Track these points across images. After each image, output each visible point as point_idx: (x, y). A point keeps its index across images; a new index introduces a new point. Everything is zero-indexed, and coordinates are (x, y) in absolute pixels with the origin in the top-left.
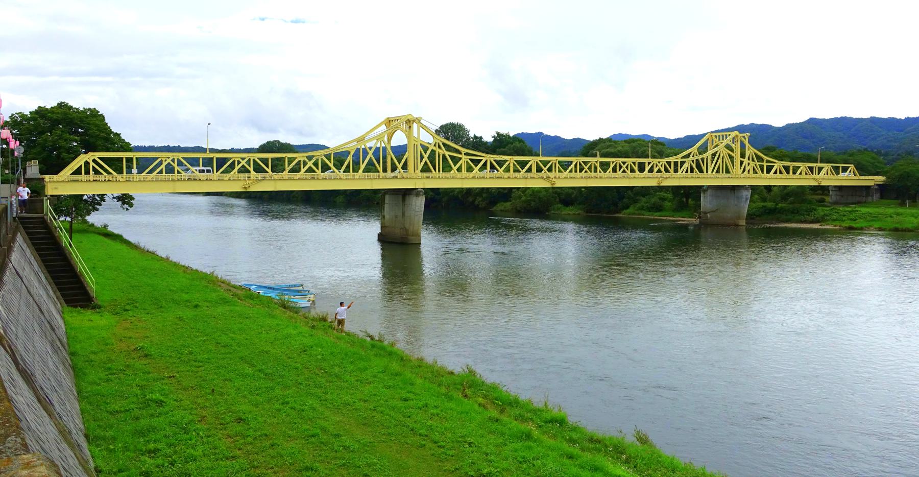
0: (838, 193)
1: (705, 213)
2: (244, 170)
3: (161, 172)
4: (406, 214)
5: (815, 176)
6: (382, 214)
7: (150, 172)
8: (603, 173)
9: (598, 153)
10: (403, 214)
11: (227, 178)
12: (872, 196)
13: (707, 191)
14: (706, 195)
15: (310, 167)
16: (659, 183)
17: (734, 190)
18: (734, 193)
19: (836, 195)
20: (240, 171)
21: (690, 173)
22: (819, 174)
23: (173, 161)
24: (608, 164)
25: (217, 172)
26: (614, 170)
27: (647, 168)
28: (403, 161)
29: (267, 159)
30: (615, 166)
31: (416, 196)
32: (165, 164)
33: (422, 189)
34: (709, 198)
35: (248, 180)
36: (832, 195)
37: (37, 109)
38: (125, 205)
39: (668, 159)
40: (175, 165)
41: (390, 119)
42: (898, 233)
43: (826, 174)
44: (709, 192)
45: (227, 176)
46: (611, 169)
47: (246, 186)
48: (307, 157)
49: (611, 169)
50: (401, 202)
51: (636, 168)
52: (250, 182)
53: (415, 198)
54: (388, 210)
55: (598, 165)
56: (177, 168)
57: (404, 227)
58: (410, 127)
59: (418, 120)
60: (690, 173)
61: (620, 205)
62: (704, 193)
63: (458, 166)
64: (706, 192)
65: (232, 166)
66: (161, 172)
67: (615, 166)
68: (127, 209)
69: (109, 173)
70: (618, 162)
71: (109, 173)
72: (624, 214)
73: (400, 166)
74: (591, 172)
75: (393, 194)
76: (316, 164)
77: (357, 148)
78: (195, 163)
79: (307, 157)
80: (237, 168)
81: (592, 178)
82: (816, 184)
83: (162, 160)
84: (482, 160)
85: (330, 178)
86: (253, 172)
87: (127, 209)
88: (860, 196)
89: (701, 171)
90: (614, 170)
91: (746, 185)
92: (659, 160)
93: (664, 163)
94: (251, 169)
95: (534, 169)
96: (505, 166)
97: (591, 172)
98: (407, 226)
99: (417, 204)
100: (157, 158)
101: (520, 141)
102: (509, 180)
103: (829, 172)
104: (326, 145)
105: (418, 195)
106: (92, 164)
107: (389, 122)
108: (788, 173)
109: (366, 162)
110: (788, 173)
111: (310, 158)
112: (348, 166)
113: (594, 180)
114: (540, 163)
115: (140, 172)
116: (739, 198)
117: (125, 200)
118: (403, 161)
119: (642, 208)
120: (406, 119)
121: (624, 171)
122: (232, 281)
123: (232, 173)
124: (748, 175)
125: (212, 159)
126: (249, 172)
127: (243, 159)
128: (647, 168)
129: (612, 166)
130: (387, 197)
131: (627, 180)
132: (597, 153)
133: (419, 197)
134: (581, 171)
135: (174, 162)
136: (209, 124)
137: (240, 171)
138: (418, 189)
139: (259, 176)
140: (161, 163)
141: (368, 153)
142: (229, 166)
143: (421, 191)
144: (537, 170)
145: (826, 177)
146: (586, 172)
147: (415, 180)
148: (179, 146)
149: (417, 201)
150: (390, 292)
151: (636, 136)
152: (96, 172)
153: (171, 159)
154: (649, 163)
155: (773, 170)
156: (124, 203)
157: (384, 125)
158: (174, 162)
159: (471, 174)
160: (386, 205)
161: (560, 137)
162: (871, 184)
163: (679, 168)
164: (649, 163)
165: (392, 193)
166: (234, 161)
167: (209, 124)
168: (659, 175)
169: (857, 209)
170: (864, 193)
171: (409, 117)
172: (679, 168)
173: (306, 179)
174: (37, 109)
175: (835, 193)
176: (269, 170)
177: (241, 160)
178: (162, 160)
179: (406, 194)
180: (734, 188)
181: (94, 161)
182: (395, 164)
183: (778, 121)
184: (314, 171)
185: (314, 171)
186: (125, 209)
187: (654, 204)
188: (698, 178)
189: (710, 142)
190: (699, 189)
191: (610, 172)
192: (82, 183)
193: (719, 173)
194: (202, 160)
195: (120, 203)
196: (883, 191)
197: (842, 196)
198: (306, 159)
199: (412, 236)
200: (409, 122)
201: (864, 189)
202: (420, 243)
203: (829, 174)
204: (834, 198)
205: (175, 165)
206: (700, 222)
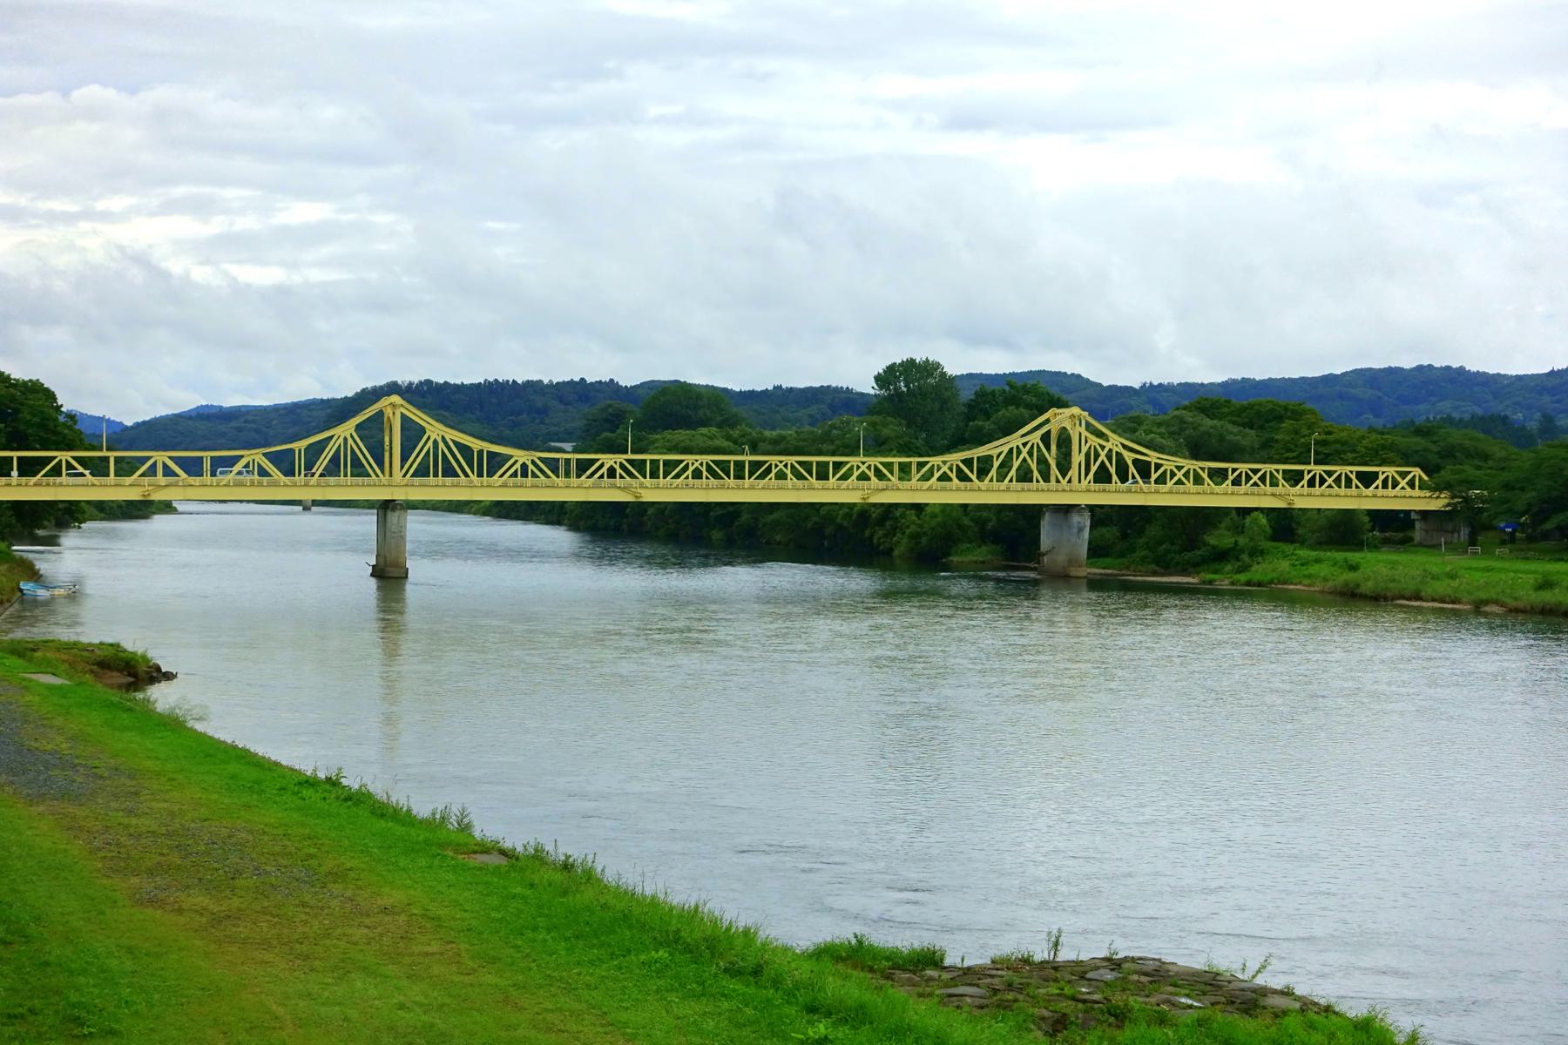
2: (863, 477)
3: (602, 476)
7: (677, 476)
11: (844, 486)
15: (1180, 479)
20: (859, 478)
21: (434, 476)
23: (701, 464)
24: (1375, 476)
25: (749, 479)
29: (891, 464)
32: (691, 469)
37: (881, 371)
40: (704, 469)
45: (762, 483)
46: (1305, 482)
48: (942, 462)
49: (1305, 482)
52: (869, 491)
55: (1353, 477)
60: (434, 476)
63: (1067, 478)
65: (769, 470)
66: (602, 476)
69: (548, 477)
70: (1344, 472)
71: (548, 477)
76: (1186, 475)
78: (125, 466)
79: (942, 462)
80: (774, 471)
81: (733, 488)
83: (688, 464)
85: (1129, 491)
86: (955, 480)
89: (1047, 479)
90: (1385, 485)
91: (1080, 505)
94: (953, 476)
97: (1340, 487)
100: (767, 462)
102: (1374, 499)
106: (531, 467)
109: (1098, 463)
111: (944, 463)
113: (735, 491)
115: (579, 476)
123: (1224, 485)
124: (1403, 493)
125: (829, 462)
126: (869, 479)
127: (697, 461)
129: (1307, 477)
131: (1256, 498)
134: (1394, 487)
135: (870, 470)
137: (859, 478)
139: (800, 483)
140: (602, 466)
141: (1028, 453)
142: (718, 467)
144: (163, 473)
146: (1330, 486)
152: (534, 475)
153: (699, 462)
154: (1309, 472)
158: (870, 470)
159: (1060, 487)
163: (519, 470)
164: (1309, 472)
166: (771, 464)
173: (442, 486)
174: (881, 371)
176: (974, 477)
177: (778, 463)
178: (688, 464)
181: (533, 462)
184: (1183, 484)
185: (1183, 484)
191: (1303, 486)
193: (1387, 488)
194: (650, 463)
198: (941, 464)
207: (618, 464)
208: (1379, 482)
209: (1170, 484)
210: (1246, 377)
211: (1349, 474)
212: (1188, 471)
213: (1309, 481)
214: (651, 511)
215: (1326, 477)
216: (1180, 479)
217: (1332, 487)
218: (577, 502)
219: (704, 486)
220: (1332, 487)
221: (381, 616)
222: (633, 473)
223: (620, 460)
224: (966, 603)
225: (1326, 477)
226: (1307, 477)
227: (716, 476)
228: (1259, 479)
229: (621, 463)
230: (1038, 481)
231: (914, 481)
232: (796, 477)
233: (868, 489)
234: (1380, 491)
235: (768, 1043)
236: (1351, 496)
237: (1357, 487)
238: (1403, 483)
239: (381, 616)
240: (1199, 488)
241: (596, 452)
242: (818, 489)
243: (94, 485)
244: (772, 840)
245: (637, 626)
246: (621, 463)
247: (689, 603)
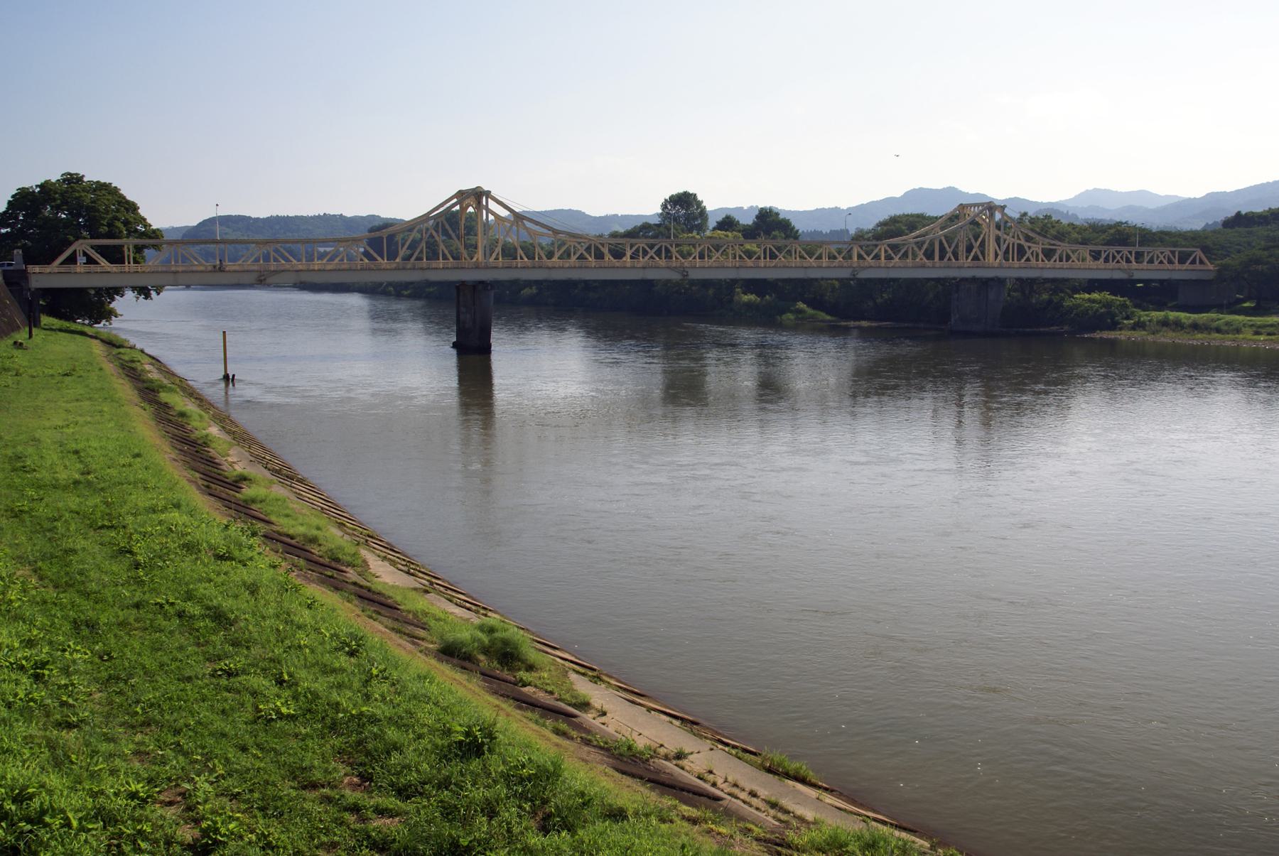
8: (1046, 262)
11: (409, 266)
26: (1106, 260)
27: (1147, 258)
28: (980, 240)
30: (1108, 255)
51: (1133, 259)
59: (488, 194)
67: (1108, 255)
74: (660, 258)
90: (1106, 260)
92: (1119, 248)
93: (641, 245)
112: (403, 246)
118: (980, 240)
121: (1118, 262)
122: (953, 446)
128: (1147, 258)
129: (1103, 256)
134: (1067, 261)
148: (684, 203)
150: (761, 395)
151: (1238, 192)
159: (774, 262)
161: (1109, 191)
163: (1189, 261)
168: (1161, 266)
172: (400, 248)
182: (944, 248)
208: (1057, 256)
209: (574, 258)
210: (32, 180)
211: (600, 247)
212: (660, 249)
213: (1105, 258)
215: (648, 249)
221: (464, 418)
222: (372, 255)
223: (643, 245)
224: (1169, 388)
225: (648, 249)
226: (1103, 256)
228: (655, 253)
230: (521, 258)
231: (1145, 263)
232: (613, 256)
234: (1191, 267)
235: (805, 855)
236: (605, 267)
238: (652, 253)
239: (464, 418)
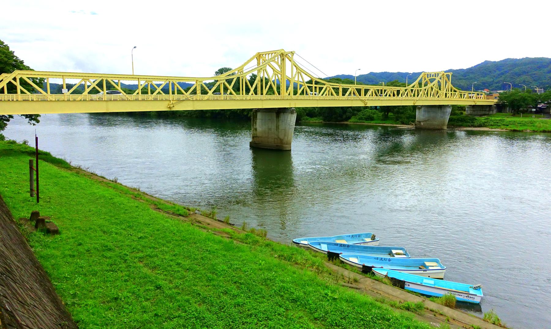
0: (471, 109)
1: (420, 122)
4: (280, 128)
5: (363, 97)
6: (254, 127)
9: (383, 83)
10: (277, 127)
12: (493, 111)
13: (421, 108)
14: (420, 111)
16: (414, 104)
17: (441, 108)
18: (441, 110)
19: (471, 110)
22: (365, 95)
31: (292, 114)
33: (294, 108)
34: (422, 113)
35: (172, 100)
36: (467, 111)
38: (32, 121)
39: (398, 88)
40: (17, 84)
41: (260, 54)
42: (545, 134)
43: (371, 95)
44: (423, 108)
47: (171, 106)
50: (275, 118)
52: (174, 102)
53: (290, 115)
54: (260, 125)
56: (19, 87)
57: (279, 138)
58: (283, 59)
61: (344, 117)
62: (419, 110)
64: (420, 109)
68: (34, 124)
72: (351, 122)
73: (252, 90)
75: (265, 112)
77: (253, 75)
82: (474, 104)
84: (323, 87)
87: (34, 124)
88: (485, 111)
95: (199, 91)
96: (207, 88)
98: (281, 137)
99: (292, 120)
101: (472, 73)
103: (374, 94)
104: (416, 71)
105: (292, 112)
107: (259, 56)
108: (337, 93)
110: (337, 93)
114: (205, 86)
116: (444, 113)
117: (33, 118)
119: (361, 119)
120: (281, 53)
130: (259, 115)
132: (382, 83)
133: (293, 114)
134: (152, 93)
136: (135, 47)
138: (291, 108)
139: (29, 95)
143: (294, 110)
144: (8, 92)
145: (371, 98)
147: (290, 101)
149: (292, 118)
155: (348, 93)
156: (30, 120)
157: (256, 58)
159: (206, 97)
160: (258, 120)
162: (492, 104)
165: (265, 111)
167: (135, 47)
169: (504, 119)
170: (488, 109)
171: (283, 52)
175: (469, 109)
179: (281, 112)
180: (440, 107)
183: (466, 66)
186: (32, 125)
187: (369, 116)
188: (378, 100)
189: (423, 79)
190: (415, 107)
191: (138, 94)
192: (33, 103)
195: (28, 119)
196: (500, 108)
197: (474, 111)
199: (287, 144)
200: (283, 56)
201: (488, 107)
202: (291, 150)
203: (373, 95)
204: (469, 112)
205: (17, 84)
206: (416, 128)
207: (18, 80)
208: (139, 90)
214: (362, 108)
216: (159, 87)
217: (161, 94)
218: (126, 112)
219: (225, 99)
220: (161, 94)
227: (32, 90)
229: (21, 79)
233: (173, 100)
237: (22, 92)
240: (113, 96)
241: (451, 81)
242: (51, 101)
243: (74, 100)
244: (321, 239)
245: (147, 186)
246: (21, 79)
247: (541, 132)
